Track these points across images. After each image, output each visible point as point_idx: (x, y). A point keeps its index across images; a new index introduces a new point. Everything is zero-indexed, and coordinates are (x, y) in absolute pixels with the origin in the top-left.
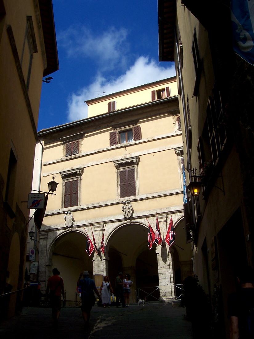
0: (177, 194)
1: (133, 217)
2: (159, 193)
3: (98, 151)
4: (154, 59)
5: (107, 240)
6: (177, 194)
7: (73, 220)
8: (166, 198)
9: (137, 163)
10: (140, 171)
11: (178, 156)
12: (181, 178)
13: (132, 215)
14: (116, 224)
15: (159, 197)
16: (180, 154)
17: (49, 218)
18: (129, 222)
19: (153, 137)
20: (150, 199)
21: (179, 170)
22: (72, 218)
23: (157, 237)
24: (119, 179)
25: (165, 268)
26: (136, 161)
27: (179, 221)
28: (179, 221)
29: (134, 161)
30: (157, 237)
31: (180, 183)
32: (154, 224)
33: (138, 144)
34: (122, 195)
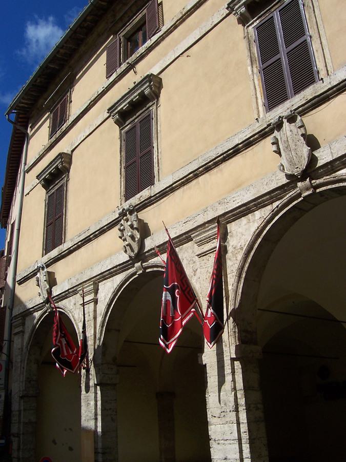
0: (248, 143)
1: (146, 250)
2: (201, 160)
3: (90, 101)
4: (36, 23)
5: (240, 277)
6: (248, 143)
7: (312, 142)
8: (221, 170)
9: (156, 95)
10: (165, 113)
11: (244, 26)
12: (257, 87)
13: (313, 160)
14: (119, 279)
15: (202, 173)
16: (248, 15)
17: (253, 148)
18: (307, 189)
19: (184, 8)
20: (183, 184)
21: (249, 68)
22: (302, 131)
23: (66, 354)
24: (123, 153)
25: (224, 420)
26: (151, 89)
27: (260, 240)
28: (260, 240)
29: (146, 92)
30: (66, 354)
31: (254, 105)
32: (194, 262)
33: (157, 43)
34: (274, 94)
